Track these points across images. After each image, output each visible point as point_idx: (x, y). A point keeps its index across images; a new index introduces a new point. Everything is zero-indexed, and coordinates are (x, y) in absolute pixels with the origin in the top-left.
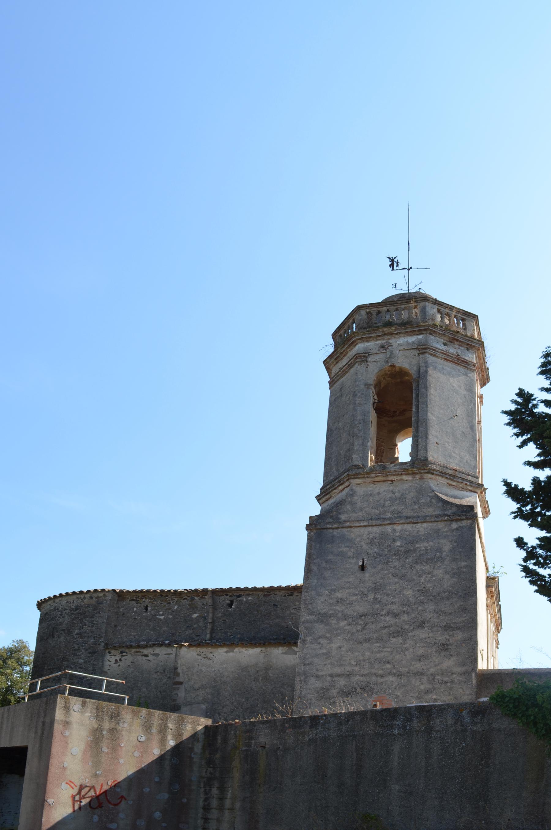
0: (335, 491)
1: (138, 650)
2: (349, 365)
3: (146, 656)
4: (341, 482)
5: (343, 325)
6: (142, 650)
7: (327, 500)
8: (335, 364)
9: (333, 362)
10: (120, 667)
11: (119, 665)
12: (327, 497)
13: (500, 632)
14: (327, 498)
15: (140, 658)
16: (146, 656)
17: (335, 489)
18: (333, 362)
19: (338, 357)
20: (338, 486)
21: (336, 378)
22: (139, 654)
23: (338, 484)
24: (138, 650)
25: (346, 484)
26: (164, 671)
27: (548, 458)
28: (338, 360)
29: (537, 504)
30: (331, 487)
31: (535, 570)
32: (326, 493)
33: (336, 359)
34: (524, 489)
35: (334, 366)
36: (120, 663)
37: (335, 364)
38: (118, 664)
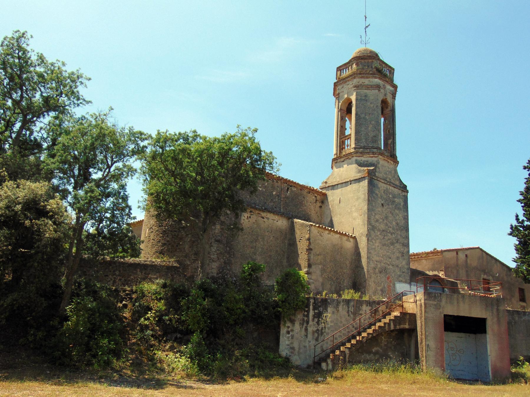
1: (259, 212)
3: (263, 218)
6: (262, 213)
10: (250, 223)
11: (249, 221)
13: (149, 134)
15: (260, 219)
16: (263, 218)
22: (259, 215)
24: (259, 212)
26: (272, 231)
27: (21, 249)
29: (19, 132)
31: (436, 275)
36: (250, 220)
38: (248, 220)
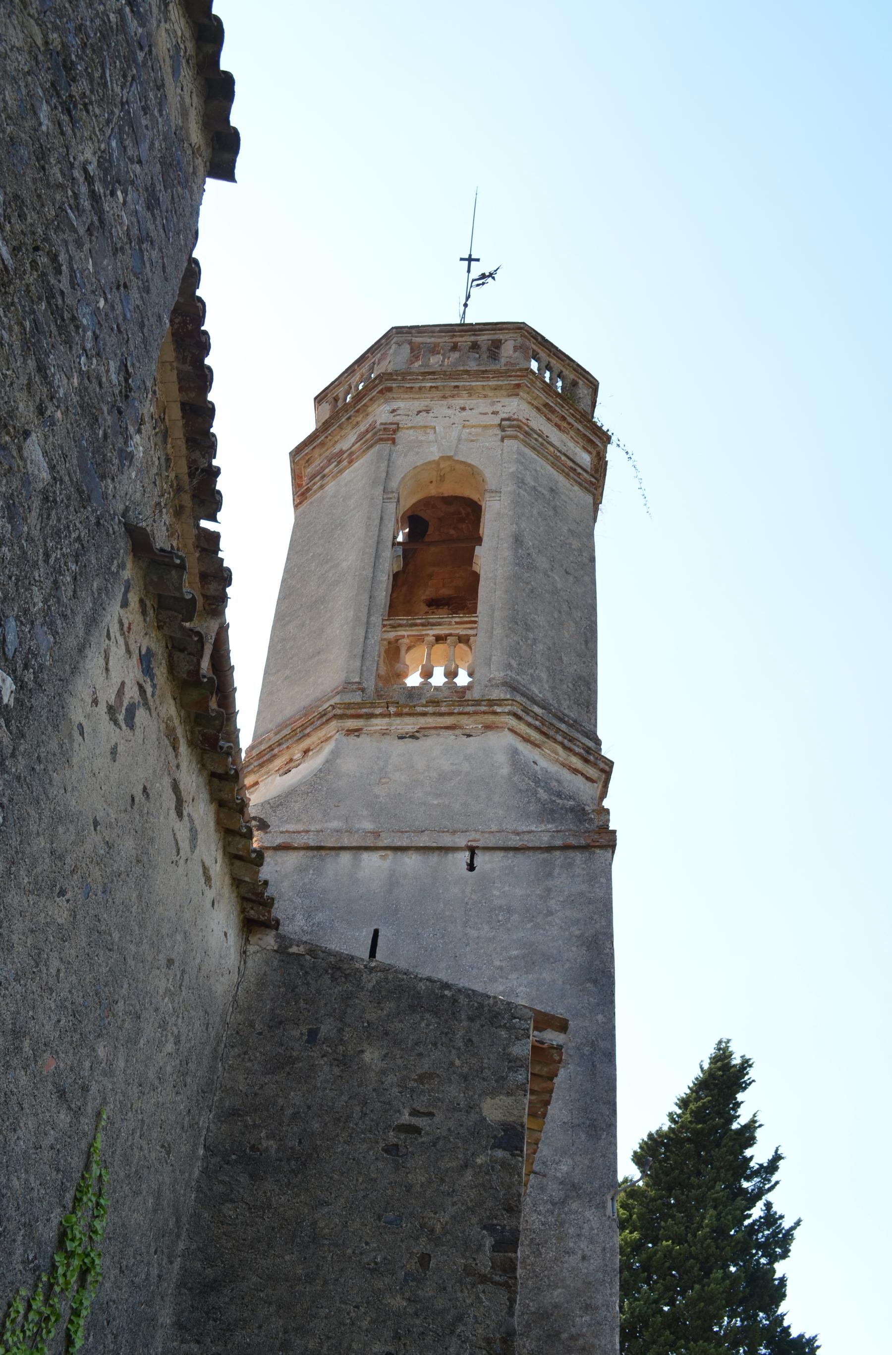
0: (559, 749)
2: (575, 470)
4: (590, 754)
5: (554, 354)
7: (526, 740)
8: (533, 405)
9: (536, 398)
12: (535, 735)
14: (530, 736)
17: (565, 747)
18: (536, 398)
19: (553, 411)
20: (576, 754)
21: (536, 440)
23: (582, 751)
25: (591, 772)
28: (544, 409)
30: (565, 735)
32: (545, 729)
33: (546, 405)
34: (635, 1153)
35: (530, 403)
37: (533, 405)
